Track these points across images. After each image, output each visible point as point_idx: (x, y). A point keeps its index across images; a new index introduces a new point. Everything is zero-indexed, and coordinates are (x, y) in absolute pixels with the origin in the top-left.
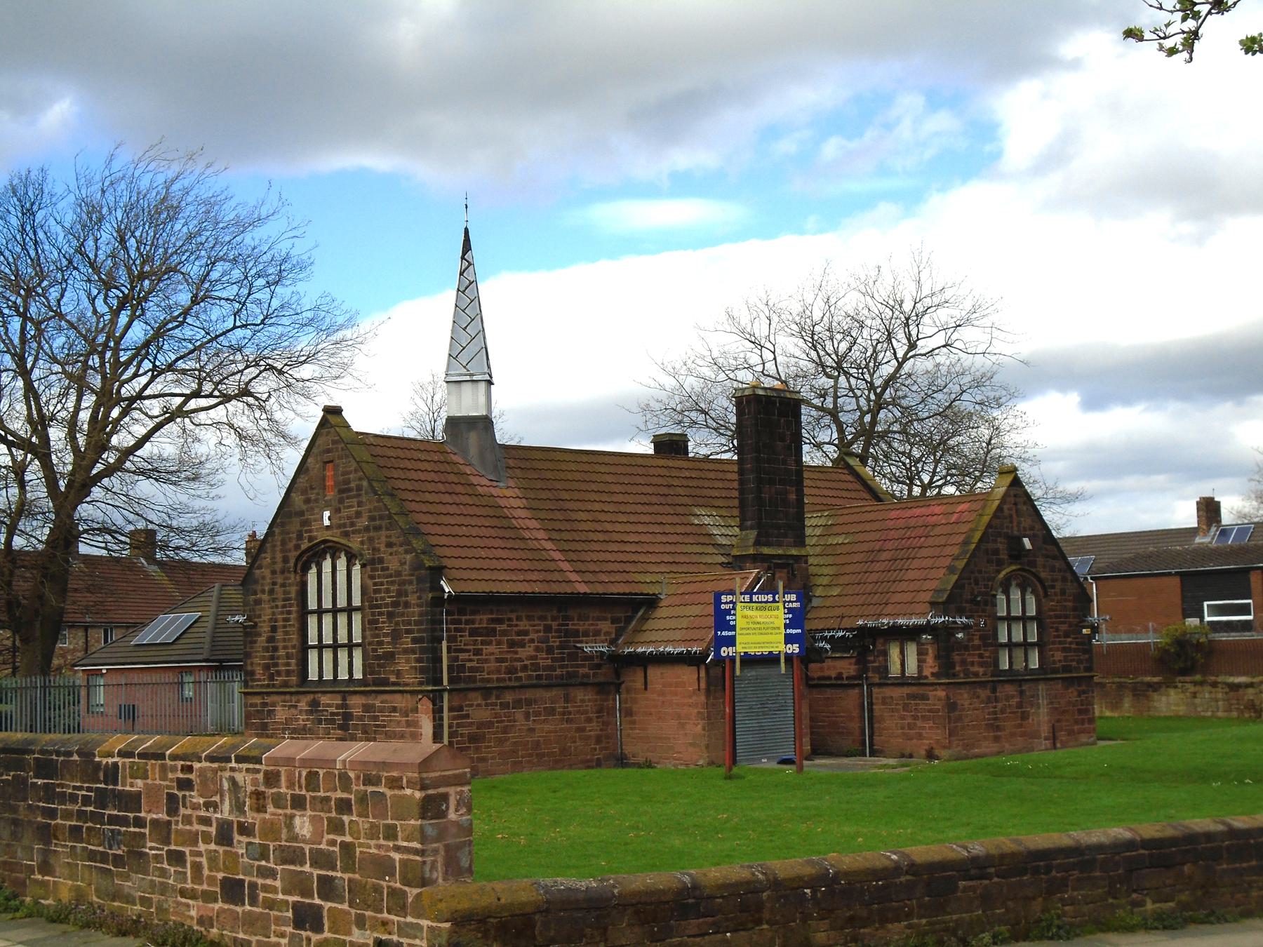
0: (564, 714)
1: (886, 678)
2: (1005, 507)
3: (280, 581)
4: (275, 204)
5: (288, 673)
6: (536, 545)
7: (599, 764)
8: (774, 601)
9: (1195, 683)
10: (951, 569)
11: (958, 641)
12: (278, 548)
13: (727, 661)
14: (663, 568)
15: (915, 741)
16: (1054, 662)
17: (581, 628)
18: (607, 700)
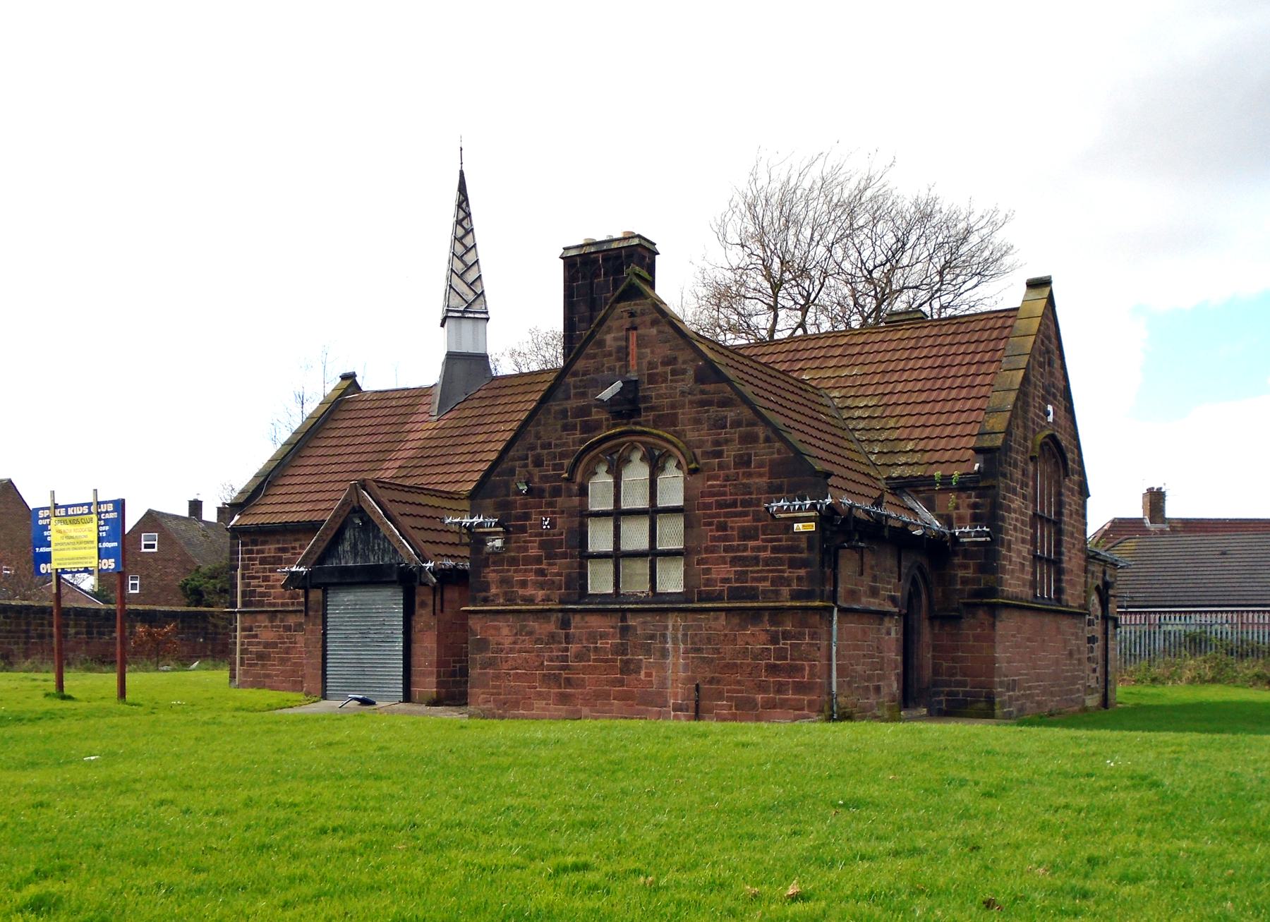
11: (495, 552)
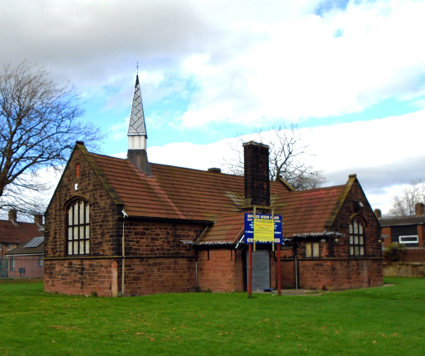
0: (174, 269)
1: (305, 257)
2: (353, 190)
3: (58, 214)
4: (71, 88)
5: (61, 251)
6: (163, 200)
7: (188, 291)
8: (270, 219)
9: (400, 265)
10: (333, 214)
12: (58, 201)
13: (250, 244)
14: (214, 212)
15: (317, 283)
16: (369, 253)
17: (182, 234)
18: (192, 264)
